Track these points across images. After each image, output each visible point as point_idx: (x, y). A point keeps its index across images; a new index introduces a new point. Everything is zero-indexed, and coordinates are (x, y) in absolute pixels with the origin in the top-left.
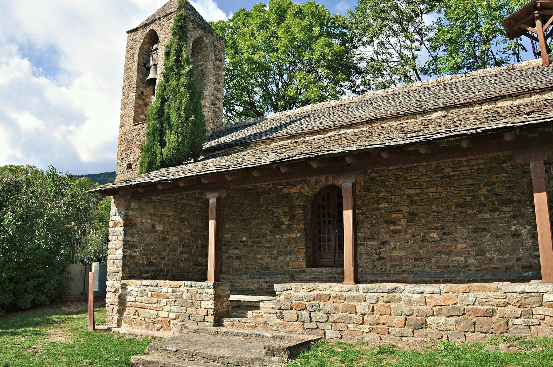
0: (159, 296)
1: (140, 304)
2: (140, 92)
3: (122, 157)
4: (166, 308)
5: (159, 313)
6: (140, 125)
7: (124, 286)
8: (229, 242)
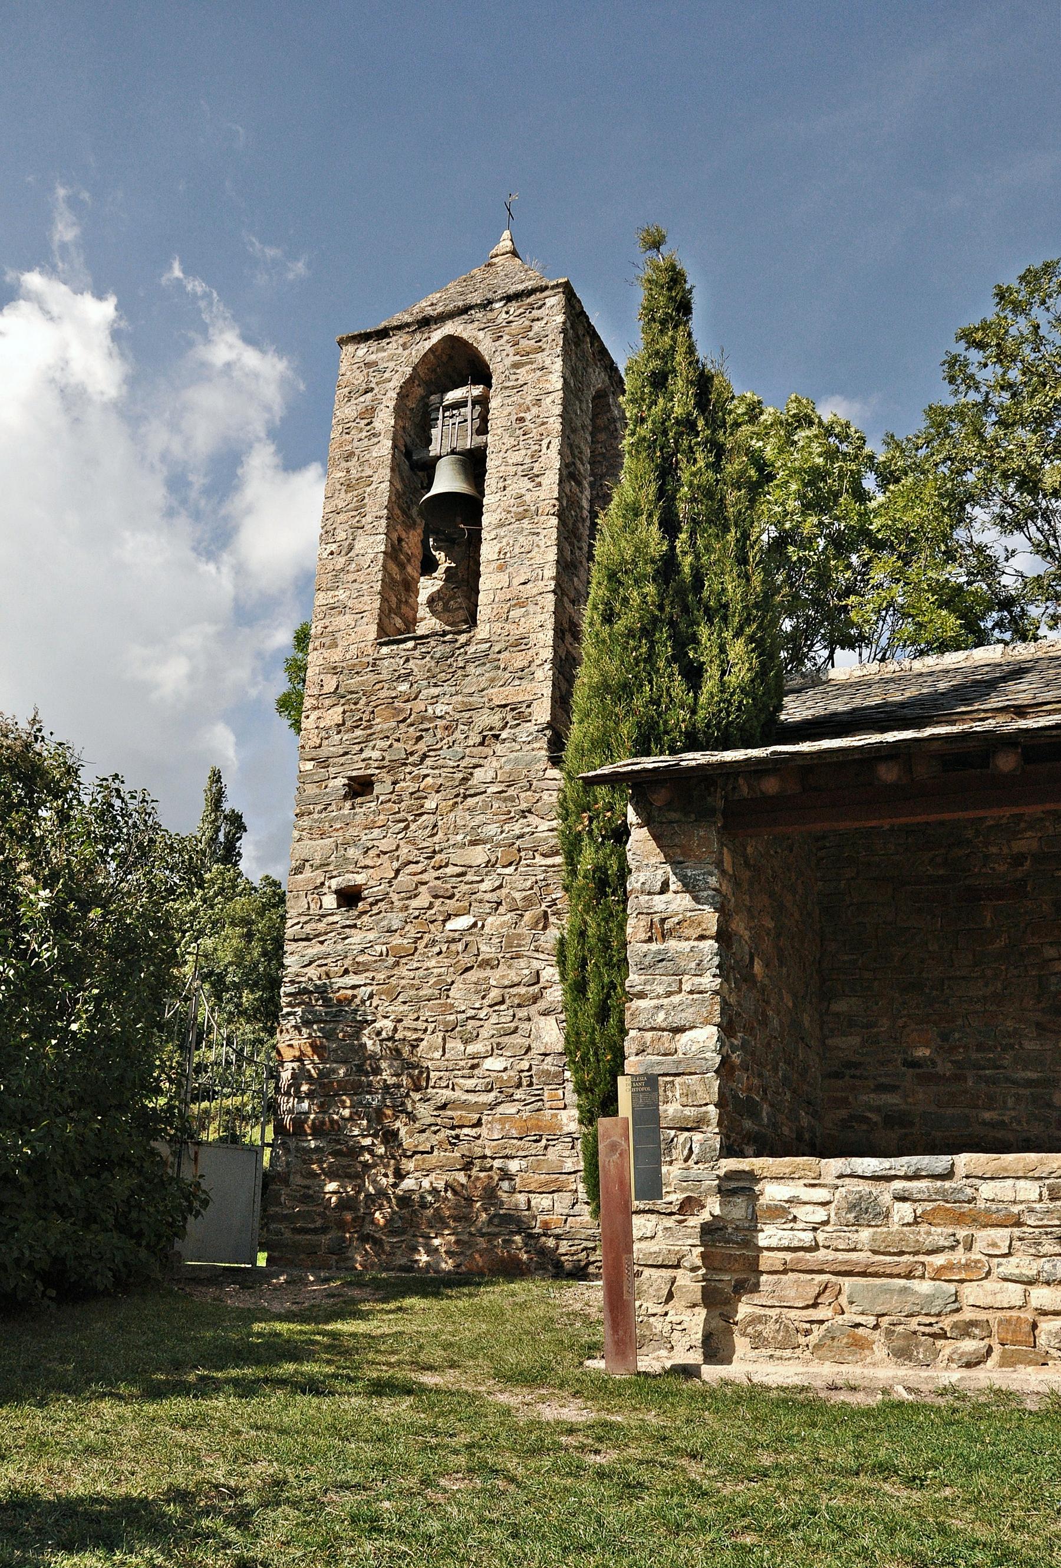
0: (960, 1219)
1: (831, 1255)
2: (395, 536)
3: (323, 752)
4: (1010, 1266)
5: (967, 1289)
6: (410, 644)
7: (738, 1187)
8: (850, 1065)
